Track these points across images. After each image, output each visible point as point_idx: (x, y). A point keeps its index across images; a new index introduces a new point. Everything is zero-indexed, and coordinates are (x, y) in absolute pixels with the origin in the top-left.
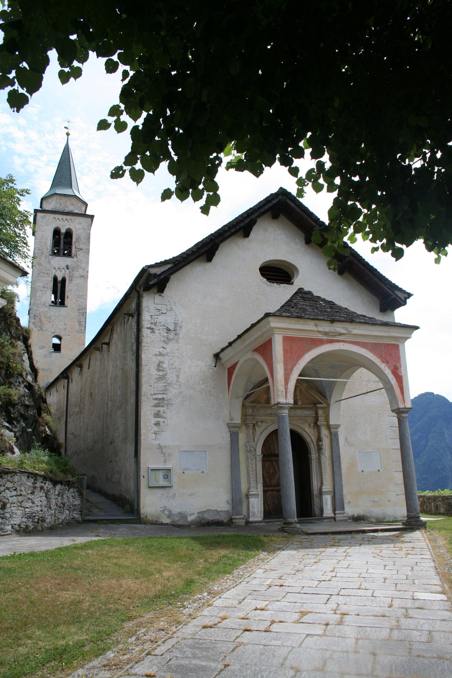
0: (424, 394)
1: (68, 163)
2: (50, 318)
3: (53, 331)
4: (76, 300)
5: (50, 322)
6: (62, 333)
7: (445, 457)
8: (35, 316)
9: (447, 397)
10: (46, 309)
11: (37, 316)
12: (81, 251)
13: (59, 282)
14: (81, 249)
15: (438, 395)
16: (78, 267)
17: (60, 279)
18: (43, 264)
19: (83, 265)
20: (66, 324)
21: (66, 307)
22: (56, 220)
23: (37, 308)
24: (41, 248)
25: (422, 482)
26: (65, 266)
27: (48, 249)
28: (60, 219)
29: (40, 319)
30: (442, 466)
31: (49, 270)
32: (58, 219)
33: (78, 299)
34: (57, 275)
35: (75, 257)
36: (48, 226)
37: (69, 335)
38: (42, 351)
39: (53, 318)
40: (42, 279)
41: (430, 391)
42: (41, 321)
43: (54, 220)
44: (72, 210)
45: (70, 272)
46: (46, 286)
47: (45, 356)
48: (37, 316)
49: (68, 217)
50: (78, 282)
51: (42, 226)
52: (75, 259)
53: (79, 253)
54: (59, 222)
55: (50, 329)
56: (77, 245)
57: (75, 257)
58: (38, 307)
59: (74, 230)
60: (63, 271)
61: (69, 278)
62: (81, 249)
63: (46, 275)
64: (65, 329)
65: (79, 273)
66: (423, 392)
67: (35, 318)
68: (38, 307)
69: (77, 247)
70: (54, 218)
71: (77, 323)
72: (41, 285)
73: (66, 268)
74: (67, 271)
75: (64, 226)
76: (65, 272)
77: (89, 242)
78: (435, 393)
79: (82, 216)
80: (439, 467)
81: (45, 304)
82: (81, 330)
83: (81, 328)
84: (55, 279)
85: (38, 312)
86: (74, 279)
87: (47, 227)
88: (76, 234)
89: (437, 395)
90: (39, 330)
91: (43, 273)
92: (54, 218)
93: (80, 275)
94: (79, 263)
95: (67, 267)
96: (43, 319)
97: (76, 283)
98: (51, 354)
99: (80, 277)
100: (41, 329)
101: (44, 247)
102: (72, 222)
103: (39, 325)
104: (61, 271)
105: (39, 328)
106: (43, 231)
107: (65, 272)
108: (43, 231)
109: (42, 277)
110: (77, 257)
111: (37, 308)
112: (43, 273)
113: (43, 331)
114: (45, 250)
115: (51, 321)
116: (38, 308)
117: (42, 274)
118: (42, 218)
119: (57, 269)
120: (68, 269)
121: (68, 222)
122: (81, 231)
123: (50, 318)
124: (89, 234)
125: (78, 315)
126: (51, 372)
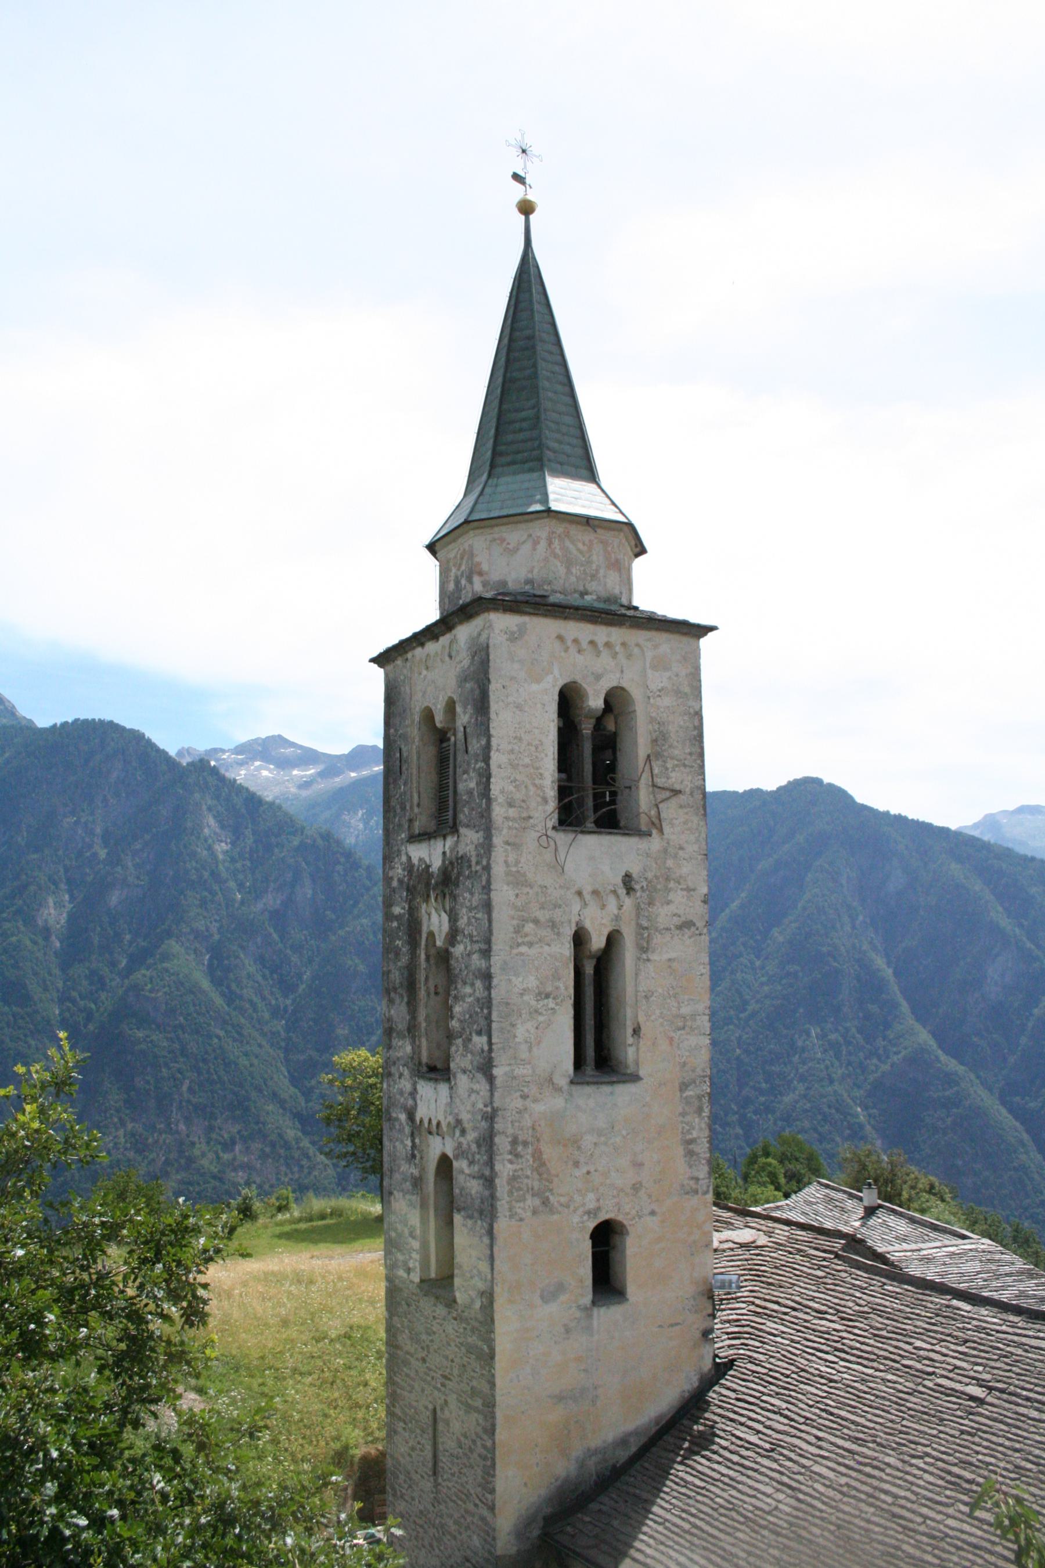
0: (800, 780)
1: (554, 349)
2: (575, 1142)
3: (591, 1205)
4: (671, 1039)
5: (576, 1164)
6: (627, 1208)
7: (838, 926)
8: (515, 1142)
9: (851, 792)
10: (558, 1102)
11: (525, 1144)
12: (674, 802)
13: (591, 957)
14: (676, 792)
15: (830, 786)
16: (668, 879)
17: (597, 942)
18: (530, 876)
19: (685, 870)
20: (638, 1165)
21: (635, 1078)
22: (566, 650)
23: (519, 1103)
24: (518, 796)
25: (784, 981)
26: (619, 880)
27: (545, 801)
28: (584, 644)
29: (537, 1155)
30: (830, 948)
31: (557, 906)
32: (576, 641)
33: (676, 1035)
34: (588, 925)
35: (654, 832)
36: (538, 681)
37: (653, 1213)
38: (553, 1308)
39: (588, 1140)
40: (533, 952)
41: (814, 775)
42: (540, 1164)
43: (557, 645)
44: (617, 591)
45: (638, 908)
46: (549, 989)
47: (568, 1331)
48: (525, 1144)
49: (602, 633)
50: (673, 955)
51: (512, 678)
52: (655, 843)
53: (670, 810)
54: (580, 659)
55: (577, 1198)
56: (656, 771)
57: (654, 832)
58: (525, 1097)
59: (636, 693)
60: (612, 904)
61: (639, 935)
62: (676, 792)
63: (546, 933)
64: (636, 1187)
65: (672, 908)
66: (799, 776)
67: (517, 1156)
68: (525, 1097)
69: (660, 781)
70: (560, 638)
71: (680, 1151)
72: (532, 982)
73: (622, 892)
74: (628, 902)
75: (598, 677)
76: (620, 907)
77: (701, 755)
78: (826, 780)
79: (667, 631)
80: (824, 949)
81: (550, 1080)
82: (697, 1179)
83: (696, 1174)
84: (579, 939)
85: (527, 1122)
86: (657, 939)
87: (535, 687)
88: (652, 720)
89: (830, 785)
90: (535, 1212)
91: (536, 921)
92: (560, 638)
93: (676, 921)
94: (670, 863)
95: (628, 881)
96: (549, 1152)
97: (666, 957)
98: (590, 1316)
99: (680, 927)
100: (546, 1202)
101: (532, 789)
102: (629, 657)
103: (536, 1185)
104: (603, 907)
105: (537, 1202)
106: (519, 707)
107: (620, 907)
108: (519, 707)
109: (530, 945)
110: (661, 831)
111: (519, 1103)
112: (536, 921)
113: (552, 1211)
114: (533, 804)
115: (582, 1160)
116: (528, 1102)
117: (529, 927)
118: (514, 637)
119: (587, 897)
120: (629, 889)
121: (615, 655)
122: (667, 701)
123: (575, 1142)
124: (698, 714)
125: (683, 1114)
126: (594, 1402)
